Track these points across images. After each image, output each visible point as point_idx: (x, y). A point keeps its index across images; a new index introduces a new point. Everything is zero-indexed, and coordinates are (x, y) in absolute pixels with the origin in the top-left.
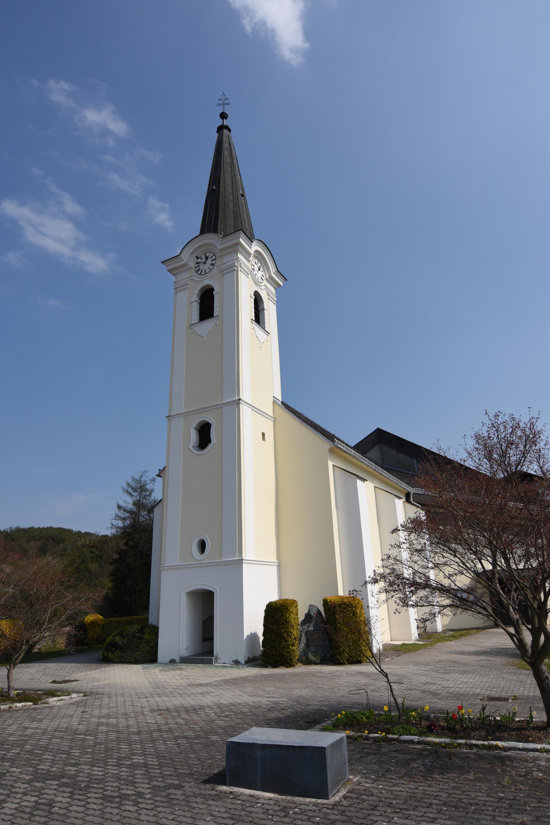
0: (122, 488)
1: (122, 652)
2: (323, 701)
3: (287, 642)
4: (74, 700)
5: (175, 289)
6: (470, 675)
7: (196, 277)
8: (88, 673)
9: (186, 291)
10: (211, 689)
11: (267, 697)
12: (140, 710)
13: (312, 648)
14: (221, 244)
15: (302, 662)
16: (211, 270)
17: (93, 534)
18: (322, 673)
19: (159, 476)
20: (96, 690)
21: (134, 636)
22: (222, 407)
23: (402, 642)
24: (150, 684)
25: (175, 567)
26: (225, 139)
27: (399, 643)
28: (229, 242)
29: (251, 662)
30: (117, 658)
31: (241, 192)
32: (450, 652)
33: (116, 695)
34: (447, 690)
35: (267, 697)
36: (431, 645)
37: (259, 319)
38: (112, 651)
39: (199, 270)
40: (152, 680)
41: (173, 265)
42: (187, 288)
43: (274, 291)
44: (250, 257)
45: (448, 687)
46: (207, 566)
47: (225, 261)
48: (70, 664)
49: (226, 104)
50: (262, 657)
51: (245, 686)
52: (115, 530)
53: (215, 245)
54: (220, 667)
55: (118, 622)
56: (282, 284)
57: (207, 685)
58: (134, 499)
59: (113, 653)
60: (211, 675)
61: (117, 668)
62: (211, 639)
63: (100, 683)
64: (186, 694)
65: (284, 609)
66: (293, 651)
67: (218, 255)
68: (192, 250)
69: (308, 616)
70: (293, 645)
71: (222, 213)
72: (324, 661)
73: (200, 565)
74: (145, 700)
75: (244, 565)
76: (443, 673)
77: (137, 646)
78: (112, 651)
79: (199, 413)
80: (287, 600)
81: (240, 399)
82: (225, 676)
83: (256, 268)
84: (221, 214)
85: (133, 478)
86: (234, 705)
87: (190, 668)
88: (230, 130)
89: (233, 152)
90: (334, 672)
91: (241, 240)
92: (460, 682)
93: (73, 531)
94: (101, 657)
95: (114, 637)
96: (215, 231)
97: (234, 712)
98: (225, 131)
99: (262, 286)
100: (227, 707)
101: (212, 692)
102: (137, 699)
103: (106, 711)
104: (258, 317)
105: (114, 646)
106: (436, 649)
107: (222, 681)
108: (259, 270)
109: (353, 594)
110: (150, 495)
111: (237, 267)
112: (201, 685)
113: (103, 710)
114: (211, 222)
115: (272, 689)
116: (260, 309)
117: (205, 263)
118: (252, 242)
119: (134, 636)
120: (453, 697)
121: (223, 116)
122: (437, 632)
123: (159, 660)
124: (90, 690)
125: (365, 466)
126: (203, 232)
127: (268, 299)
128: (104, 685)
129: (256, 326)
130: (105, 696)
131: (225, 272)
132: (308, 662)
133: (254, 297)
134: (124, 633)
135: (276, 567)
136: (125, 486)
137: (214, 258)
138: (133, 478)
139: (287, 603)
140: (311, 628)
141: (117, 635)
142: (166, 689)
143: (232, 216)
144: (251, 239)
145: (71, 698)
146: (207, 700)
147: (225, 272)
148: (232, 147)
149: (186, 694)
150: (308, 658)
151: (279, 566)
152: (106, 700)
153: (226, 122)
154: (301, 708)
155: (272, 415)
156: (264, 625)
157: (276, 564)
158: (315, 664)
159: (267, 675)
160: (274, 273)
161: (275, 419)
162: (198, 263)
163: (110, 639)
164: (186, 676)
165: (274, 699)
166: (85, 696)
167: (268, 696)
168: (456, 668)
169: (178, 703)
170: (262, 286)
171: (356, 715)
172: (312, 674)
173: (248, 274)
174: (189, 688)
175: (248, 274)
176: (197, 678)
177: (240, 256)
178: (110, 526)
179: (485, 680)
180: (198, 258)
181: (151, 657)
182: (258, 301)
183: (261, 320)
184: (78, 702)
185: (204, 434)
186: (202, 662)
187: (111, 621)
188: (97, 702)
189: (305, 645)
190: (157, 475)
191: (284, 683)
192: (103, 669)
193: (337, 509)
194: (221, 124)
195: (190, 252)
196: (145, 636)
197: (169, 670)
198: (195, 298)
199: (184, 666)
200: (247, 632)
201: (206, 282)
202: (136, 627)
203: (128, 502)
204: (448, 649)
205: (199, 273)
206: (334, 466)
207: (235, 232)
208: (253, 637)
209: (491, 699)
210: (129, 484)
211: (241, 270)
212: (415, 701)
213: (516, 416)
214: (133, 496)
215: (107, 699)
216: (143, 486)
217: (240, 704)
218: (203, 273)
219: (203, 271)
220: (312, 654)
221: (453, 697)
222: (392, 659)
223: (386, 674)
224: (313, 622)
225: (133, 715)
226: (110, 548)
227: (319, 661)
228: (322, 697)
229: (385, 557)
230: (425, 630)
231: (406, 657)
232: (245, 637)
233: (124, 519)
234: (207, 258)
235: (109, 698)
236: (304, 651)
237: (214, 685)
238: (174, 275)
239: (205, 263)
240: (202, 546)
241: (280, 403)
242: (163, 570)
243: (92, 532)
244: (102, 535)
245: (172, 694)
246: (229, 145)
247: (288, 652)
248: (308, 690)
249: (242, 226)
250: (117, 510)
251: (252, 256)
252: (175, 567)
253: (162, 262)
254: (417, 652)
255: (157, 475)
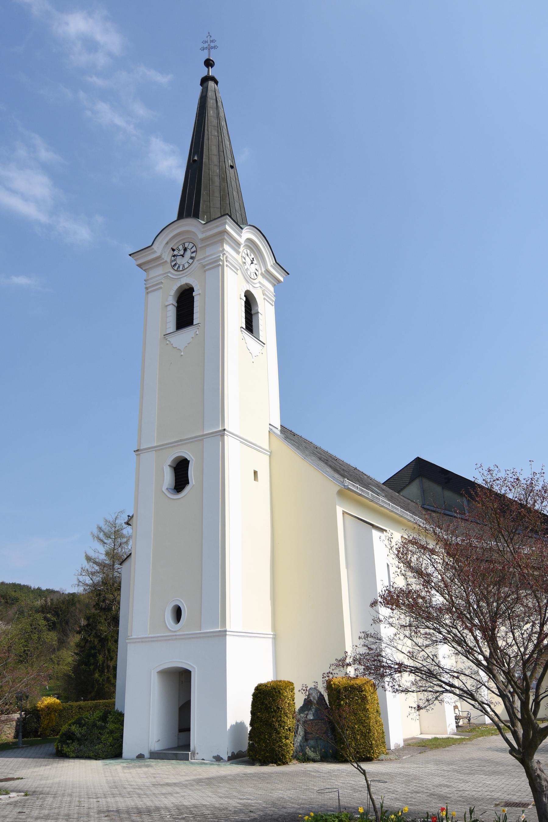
0: (92, 533)
1: (80, 745)
2: (304, 804)
3: (279, 734)
4: (12, 800)
5: (147, 288)
6: (497, 777)
7: (173, 274)
8: (37, 769)
9: (161, 290)
10: (177, 789)
11: (240, 799)
12: (86, 811)
13: (312, 742)
14: (203, 232)
15: (298, 759)
16: (191, 264)
17: (57, 592)
18: (318, 772)
19: (128, 523)
20: (41, 789)
21: (94, 725)
22: (202, 440)
23: (433, 736)
24: (107, 782)
25: (143, 640)
26: (210, 94)
27: (430, 737)
28: (213, 229)
29: (236, 758)
30: (73, 752)
31: (230, 162)
32: (490, 749)
33: (63, 795)
34: (460, 793)
35: (240, 799)
36: (470, 739)
37: (252, 326)
38: (67, 744)
39: (175, 265)
40: (111, 778)
41: (143, 257)
42: (161, 288)
43: (272, 289)
44: (240, 248)
45: (463, 790)
46: (208, 637)
47: (207, 254)
48: (16, 759)
49: (212, 48)
50: (248, 752)
51: (219, 787)
52: (82, 588)
53: (196, 234)
54: (198, 764)
55: (80, 708)
56: (282, 279)
57: (175, 784)
58: (107, 547)
59: (68, 746)
60: (183, 774)
61: (72, 764)
62: (188, 730)
63: (48, 782)
64: (145, 794)
65: (276, 692)
66: (286, 745)
67: (200, 246)
68: (167, 239)
69: (308, 703)
70: (287, 738)
71: (205, 193)
72: (325, 759)
73: (174, 637)
74: (95, 800)
75: (227, 637)
76: (465, 774)
77: (98, 738)
78: (67, 744)
79: (173, 447)
80: (280, 681)
81: (224, 430)
82: (200, 775)
83: (248, 261)
84: (203, 193)
85: (106, 521)
86: (196, 807)
87: (160, 764)
88: (216, 82)
89: (221, 110)
90: (334, 771)
91: (227, 227)
92: (480, 785)
93: (31, 588)
94: (55, 751)
95: (70, 726)
96: (196, 216)
97: (192, 814)
98: (211, 84)
99: (255, 284)
100: (187, 808)
101: (177, 793)
102: (86, 800)
103: (46, 812)
104: (250, 324)
105: (69, 737)
106: (473, 744)
107: (194, 780)
108: (252, 263)
109: (329, 676)
110: (127, 543)
111: (223, 261)
112: (168, 785)
113: (43, 811)
114: (191, 204)
115: (250, 790)
116: (253, 312)
117: (183, 256)
118: (242, 228)
119: (94, 725)
120: (464, 802)
121: (209, 63)
122: (485, 724)
123: (124, 755)
124: (33, 790)
125: (388, 512)
126: (181, 216)
127: (264, 299)
128: (52, 784)
129: (247, 335)
130: (50, 796)
131: (207, 268)
132: (306, 759)
133: (244, 299)
134: (83, 721)
135: (271, 640)
136: (96, 531)
137: (194, 249)
138: (106, 521)
139: (280, 686)
140: (311, 717)
141: (74, 723)
142: (125, 788)
143: (217, 194)
144: (240, 223)
145: (9, 797)
146: (168, 802)
147: (207, 268)
148: (220, 104)
149: (145, 794)
150: (306, 754)
151: (275, 638)
152: (49, 800)
153: (212, 72)
154: (273, 811)
155: (267, 448)
156: (252, 713)
157: (271, 636)
158: (314, 761)
159: (251, 774)
160: (271, 266)
161: (271, 452)
162: (174, 256)
163: (64, 728)
164: (153, 774)
165: (247, 801)
166: (26, 795)
167: (242, 797)
168: (485, 768)
169: (133, 804)
170: (255, 284)
171: (328, 817)
172: (306, 774)
173: (237, 270)
174: (152, 788)
175: (237, 270)
176: (166, 776)
177: (227, 247)
178: (77, 583)
179: (512, 783)
180: (173, 250)
181: (115, 752)
182: (250, 303)
183: (254, 327)
184: (16, 802)
185: (181, 472)
186: (176, 757)
187: (72, 706)
188: (38, 803)
189: (302, 738)
190: (125, 523)
191: (268, 783)
192: (55, 765)
193: (347, 567)
194: (206, 74)
195: (165, 242)
196: (108, 725)
197: (134, 767)
198: (171, 301)
199: (153, 762)
200: (231, 721)
201: (184, 281)
202: (98, 714)
203: (100, 552)
204: (488, 745)
205: (176, 269)
206: (344, 513)
207: (221, 216)
208: (239, 726)
209: (508, 804)
210: (100, 529)
211: (227, 266)
212: (415, 805)
213: (518, 470)
214: (105, 543)
215: (51, 799)
216: (118, 531)
217: (204, 805)
218: (181, 269)
219: (181, 267)
220: (310, 749)
221: (464, 802)
222: (412, 756)
223: (364, 771)
224: (313, 710)
225: (76, 816)
226: (77, 610)
227: (319, 758)
228: (305, 800)
229: (363, 635)
230: (469, 720)
231: (431, 755)
232: (228, 727)
233: (93, 574)
234: (185, 250)
235: (54, 797)
236: (300, 745)
237: (183, 785)
238: (144, 270)
239: (183, 256)
240: (178, 613)
241: (279, 433)
242: (130, 643)
243: (56, 589)
244: (69, 593)
245: (129, 794)
246: (215, 101)
247: (280, 747)
248: (293, 791)
249: (231, 209)
250: (86, 562)
251: (242, 246)
252: (143, 640)
253: (130, 255)
254: (447, 748)
255: (125, 523)
